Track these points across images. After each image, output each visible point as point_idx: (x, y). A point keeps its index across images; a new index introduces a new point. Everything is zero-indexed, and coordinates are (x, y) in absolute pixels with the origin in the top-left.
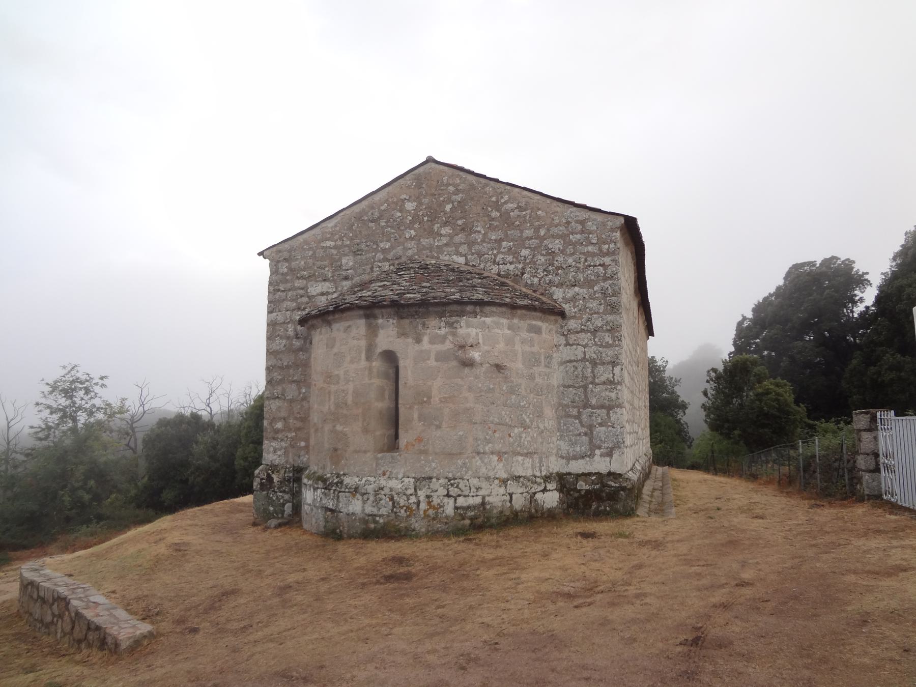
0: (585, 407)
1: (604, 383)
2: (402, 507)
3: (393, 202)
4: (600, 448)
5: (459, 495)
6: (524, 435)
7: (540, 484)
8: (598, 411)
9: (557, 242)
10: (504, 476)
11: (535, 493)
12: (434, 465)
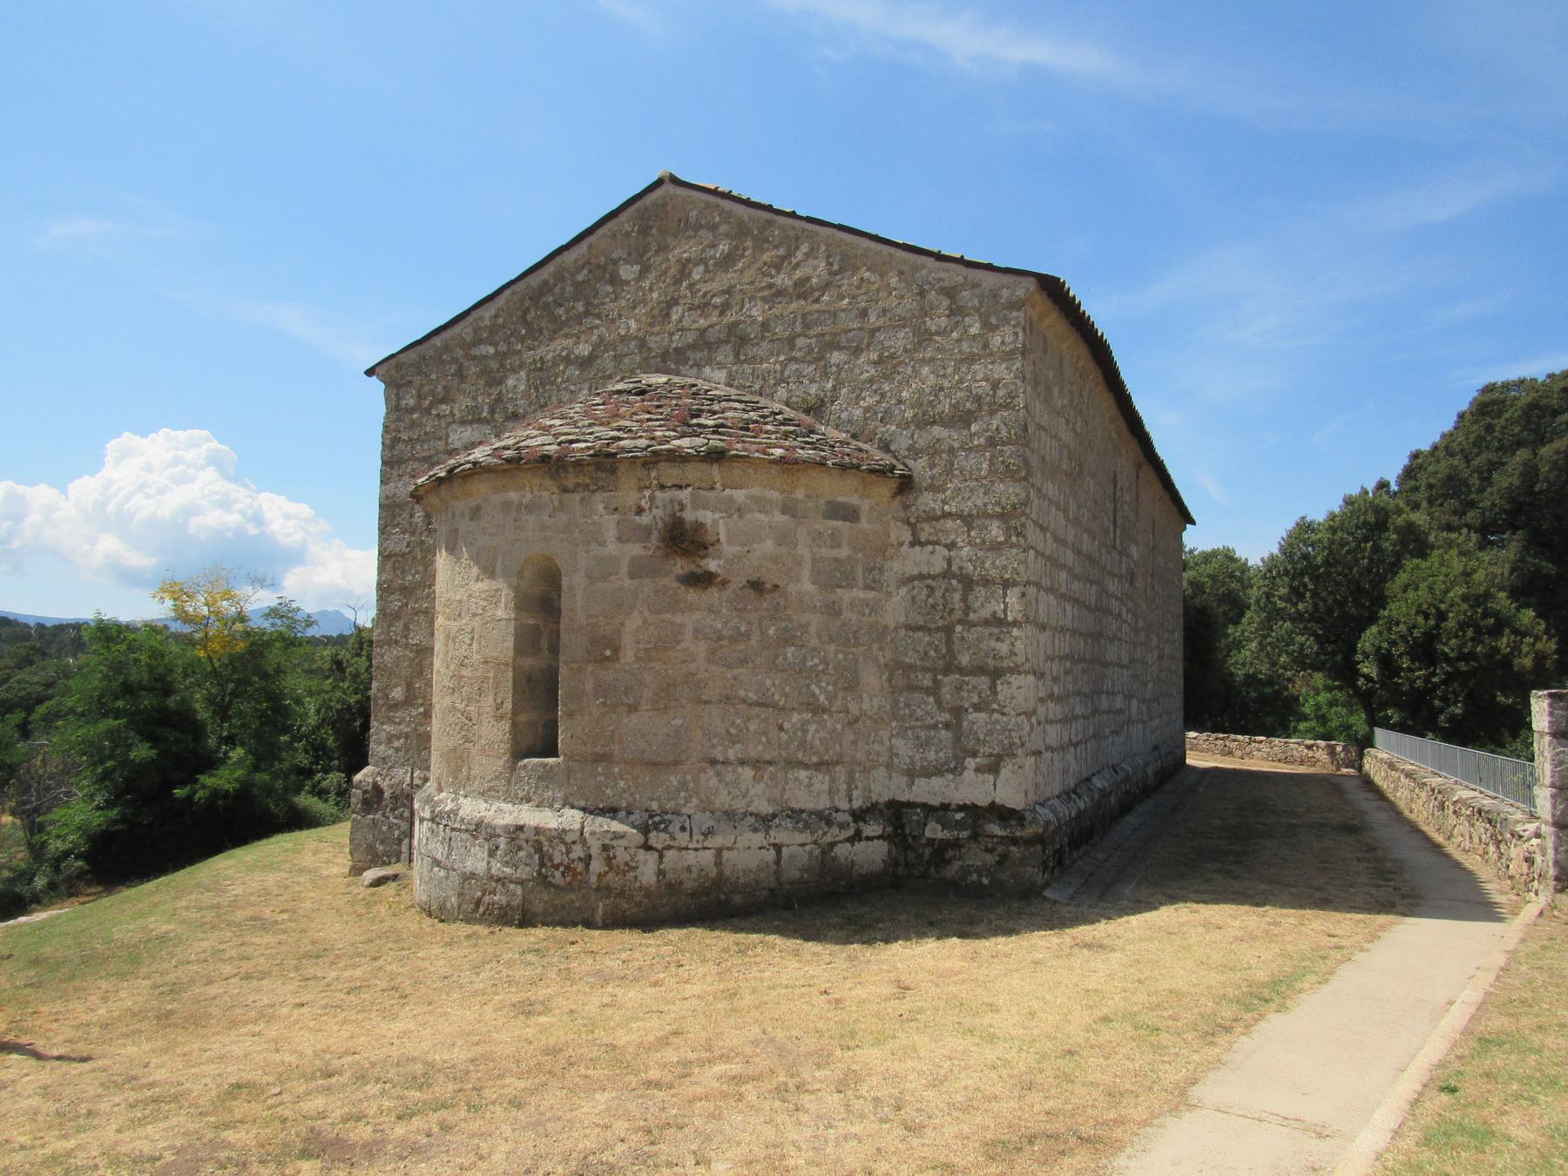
0: (947, 671)
1: (987, 623)
2: (557, 867)
3: (599, 267)
4: (974, 754)
5: (669, 847)
6: (813, 728)
7: (843, 826)
8: (973, 680)
9: (901, 334)
10: (766, 809)
11: (833, 845)
12: (622, 784)
